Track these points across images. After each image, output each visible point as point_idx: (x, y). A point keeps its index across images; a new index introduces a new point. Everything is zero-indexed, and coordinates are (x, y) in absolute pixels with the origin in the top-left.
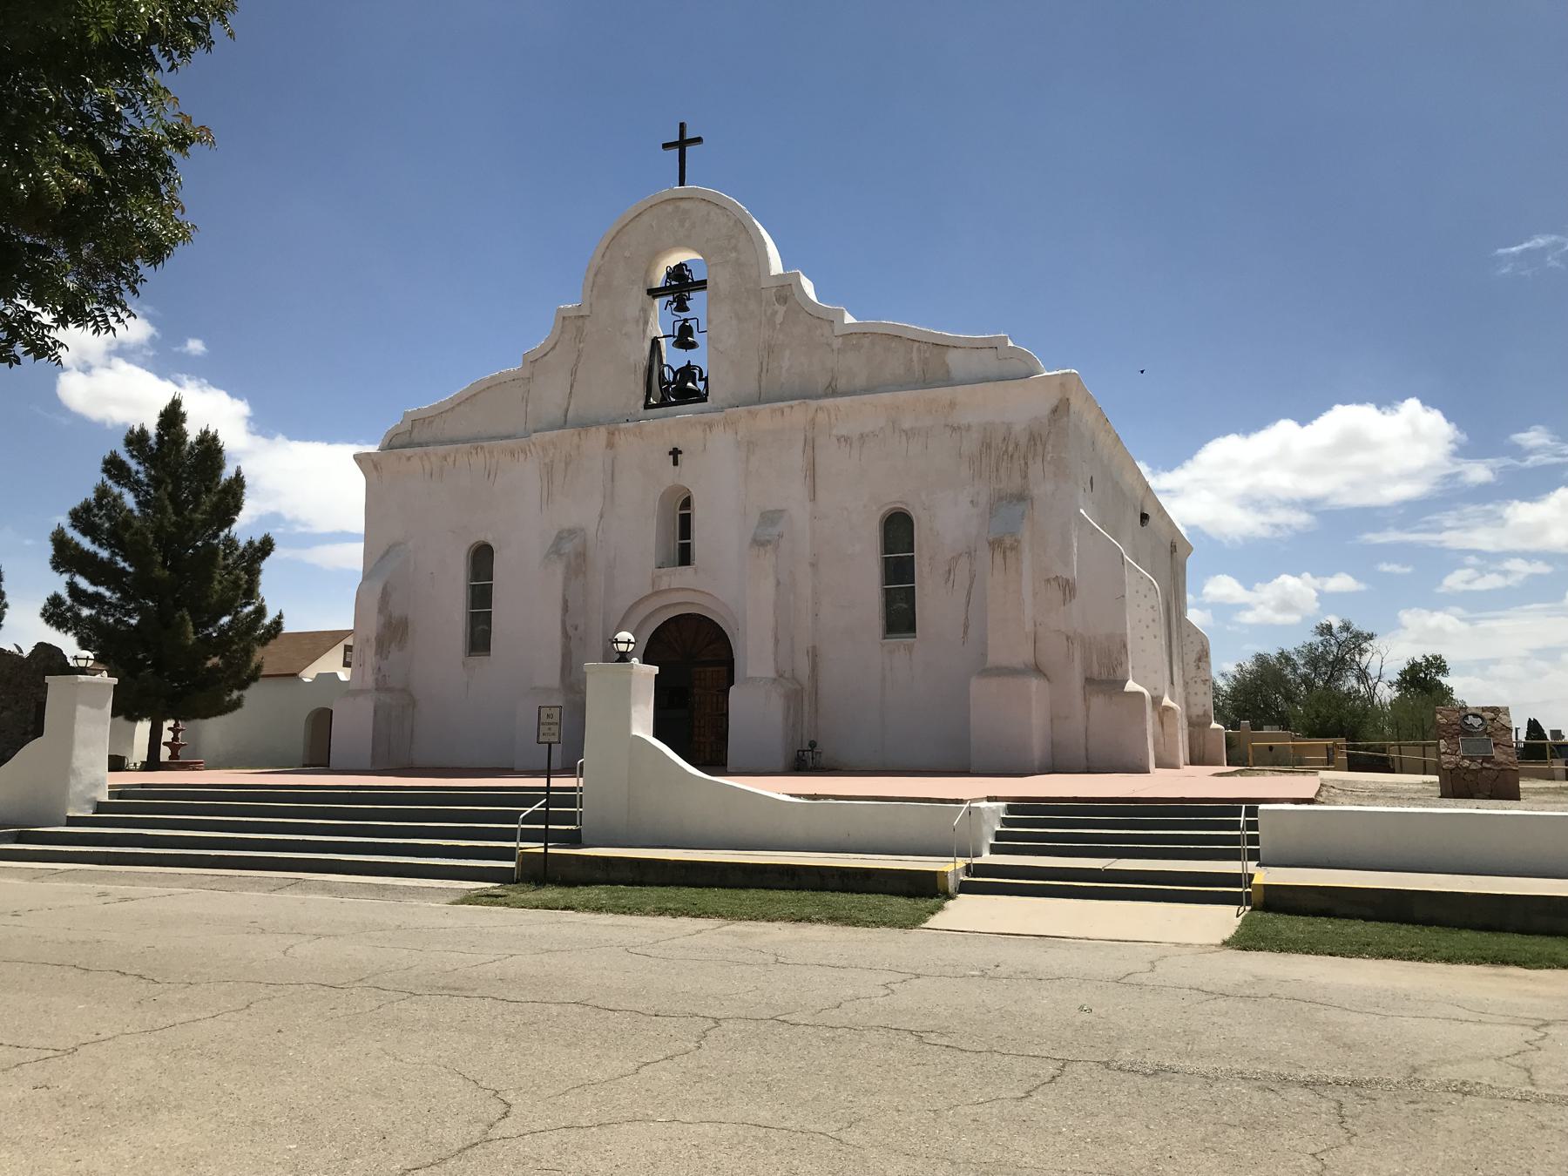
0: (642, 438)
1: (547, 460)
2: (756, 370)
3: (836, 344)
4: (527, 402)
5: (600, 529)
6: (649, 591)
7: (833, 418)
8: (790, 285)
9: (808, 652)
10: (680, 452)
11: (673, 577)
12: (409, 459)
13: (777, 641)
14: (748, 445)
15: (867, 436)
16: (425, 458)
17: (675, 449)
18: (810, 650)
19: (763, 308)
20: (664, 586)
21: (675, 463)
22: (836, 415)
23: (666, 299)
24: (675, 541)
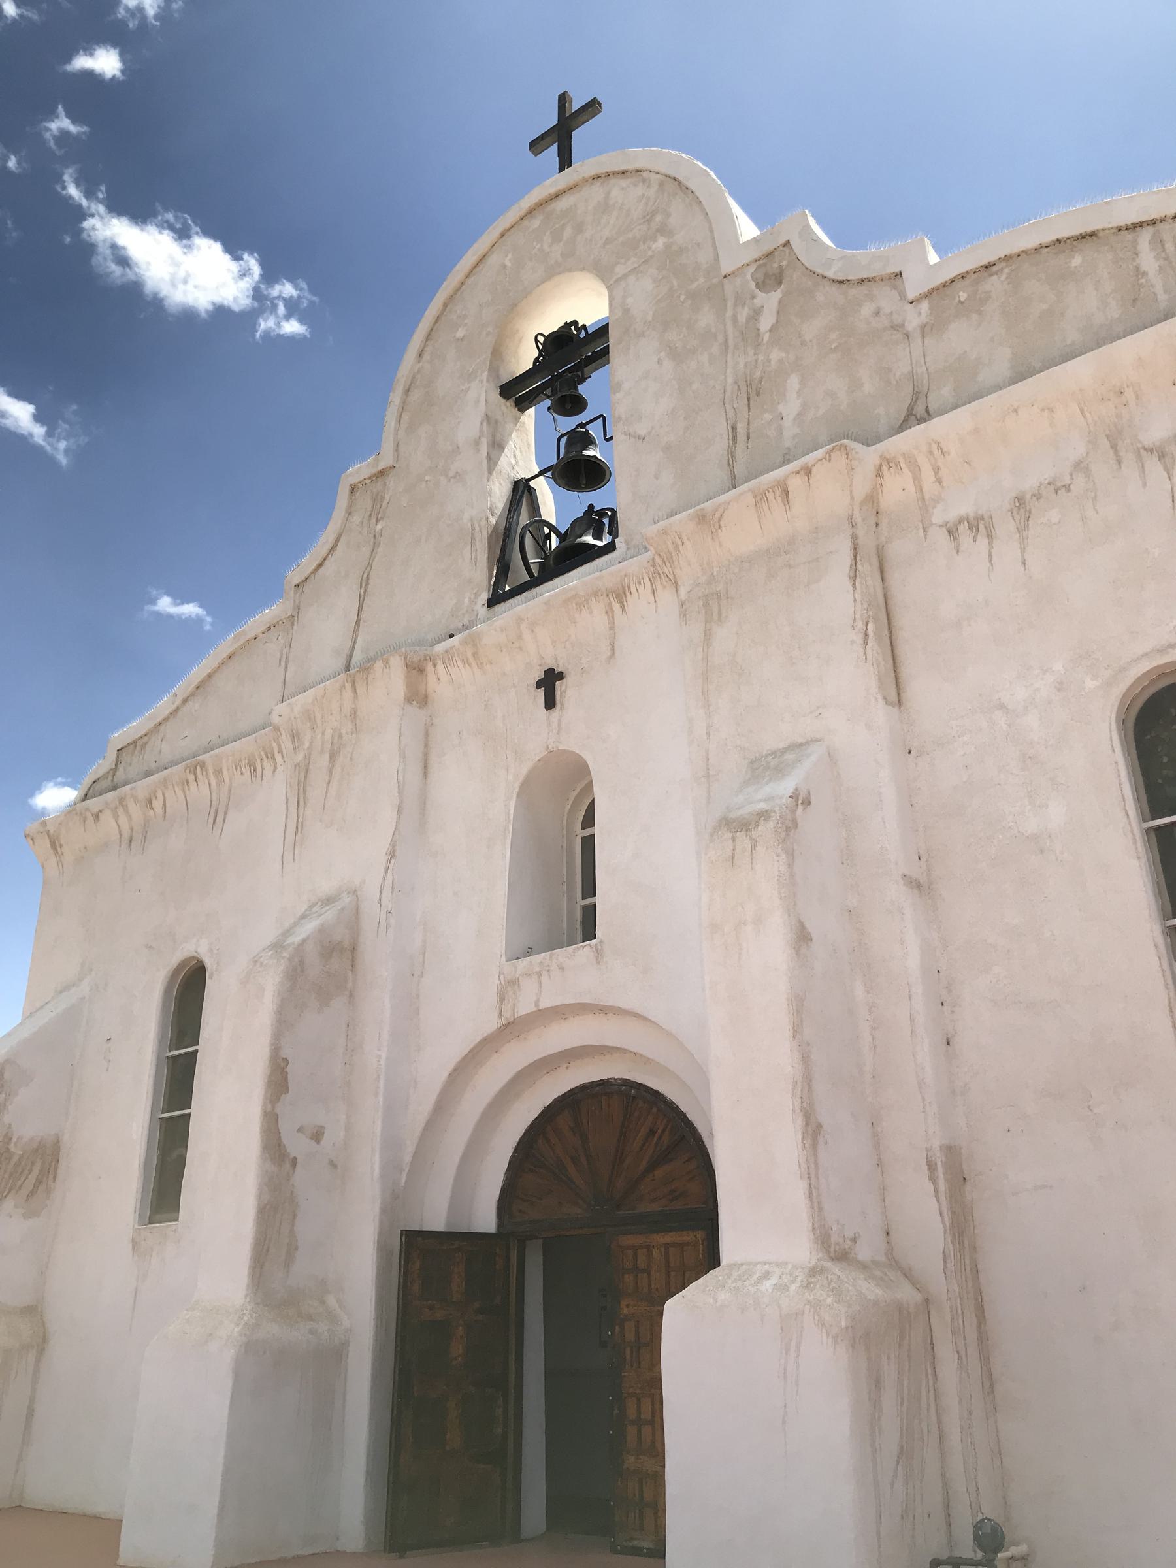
0: (480, 665)
1: (300, 757)
2: (722, 444)
3: (914, 318)
4: (286, 663)
5: (388, 883)
6: (491, 1024)
7: (928, 476)
8: (787, 244)
9: (931, 1166)
10: (561, 676)
11: (545, 979)
12: (97, 817)
13: (813, 1131)
14: (706, 605)
15: (1037, 496)
16: (120, 811)
18: (939, 1158)
19: (729, 314)
20: (525, 1006)
21: (550, 703)
22: (937, 470)
24: (571, 899)
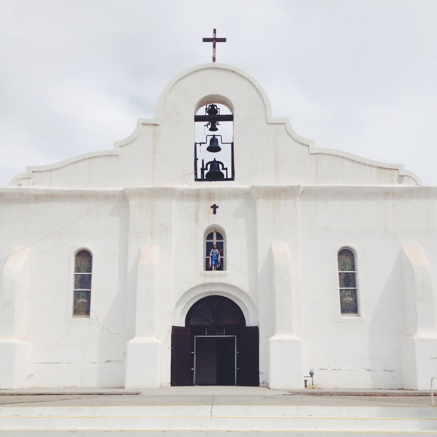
10: (218, 207)
17: (215, 205)
21: (215, 213)
23: (206, 123)
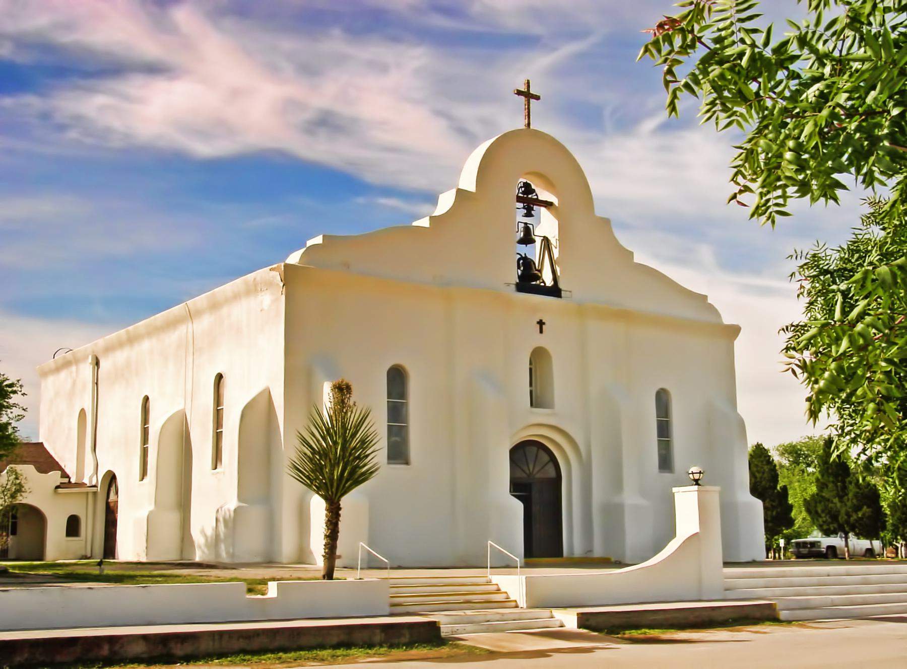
21: (541, 331)
